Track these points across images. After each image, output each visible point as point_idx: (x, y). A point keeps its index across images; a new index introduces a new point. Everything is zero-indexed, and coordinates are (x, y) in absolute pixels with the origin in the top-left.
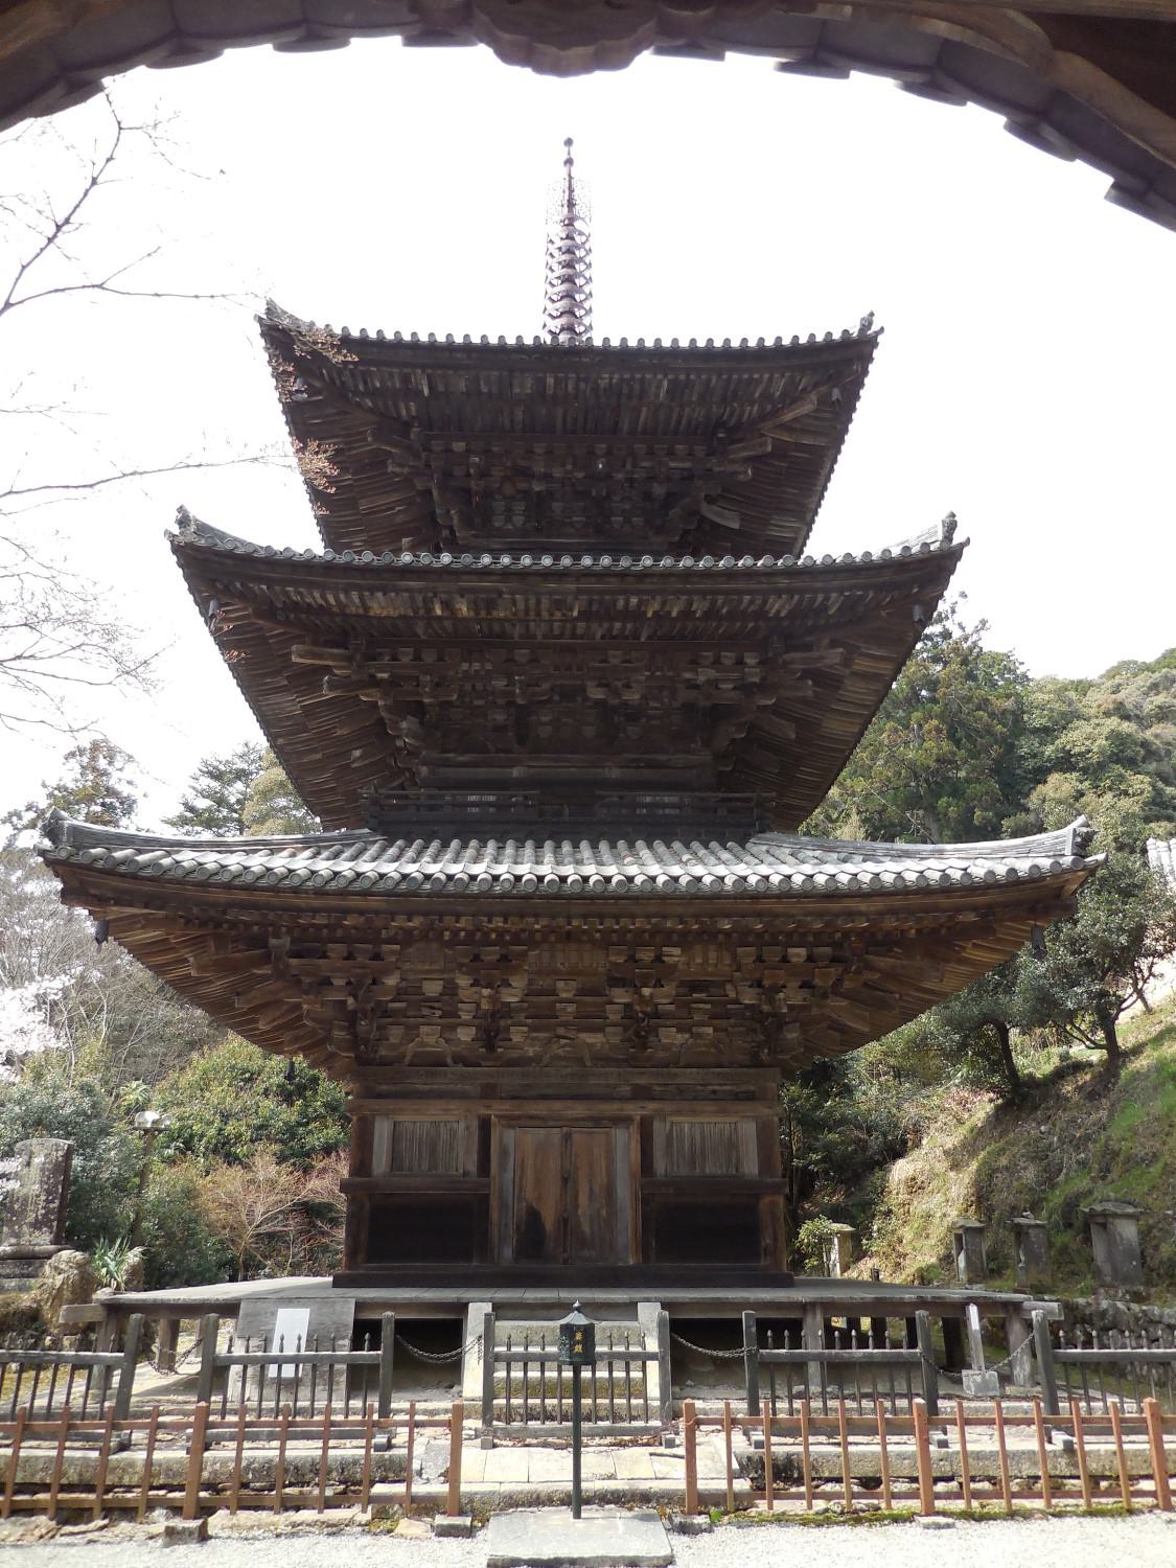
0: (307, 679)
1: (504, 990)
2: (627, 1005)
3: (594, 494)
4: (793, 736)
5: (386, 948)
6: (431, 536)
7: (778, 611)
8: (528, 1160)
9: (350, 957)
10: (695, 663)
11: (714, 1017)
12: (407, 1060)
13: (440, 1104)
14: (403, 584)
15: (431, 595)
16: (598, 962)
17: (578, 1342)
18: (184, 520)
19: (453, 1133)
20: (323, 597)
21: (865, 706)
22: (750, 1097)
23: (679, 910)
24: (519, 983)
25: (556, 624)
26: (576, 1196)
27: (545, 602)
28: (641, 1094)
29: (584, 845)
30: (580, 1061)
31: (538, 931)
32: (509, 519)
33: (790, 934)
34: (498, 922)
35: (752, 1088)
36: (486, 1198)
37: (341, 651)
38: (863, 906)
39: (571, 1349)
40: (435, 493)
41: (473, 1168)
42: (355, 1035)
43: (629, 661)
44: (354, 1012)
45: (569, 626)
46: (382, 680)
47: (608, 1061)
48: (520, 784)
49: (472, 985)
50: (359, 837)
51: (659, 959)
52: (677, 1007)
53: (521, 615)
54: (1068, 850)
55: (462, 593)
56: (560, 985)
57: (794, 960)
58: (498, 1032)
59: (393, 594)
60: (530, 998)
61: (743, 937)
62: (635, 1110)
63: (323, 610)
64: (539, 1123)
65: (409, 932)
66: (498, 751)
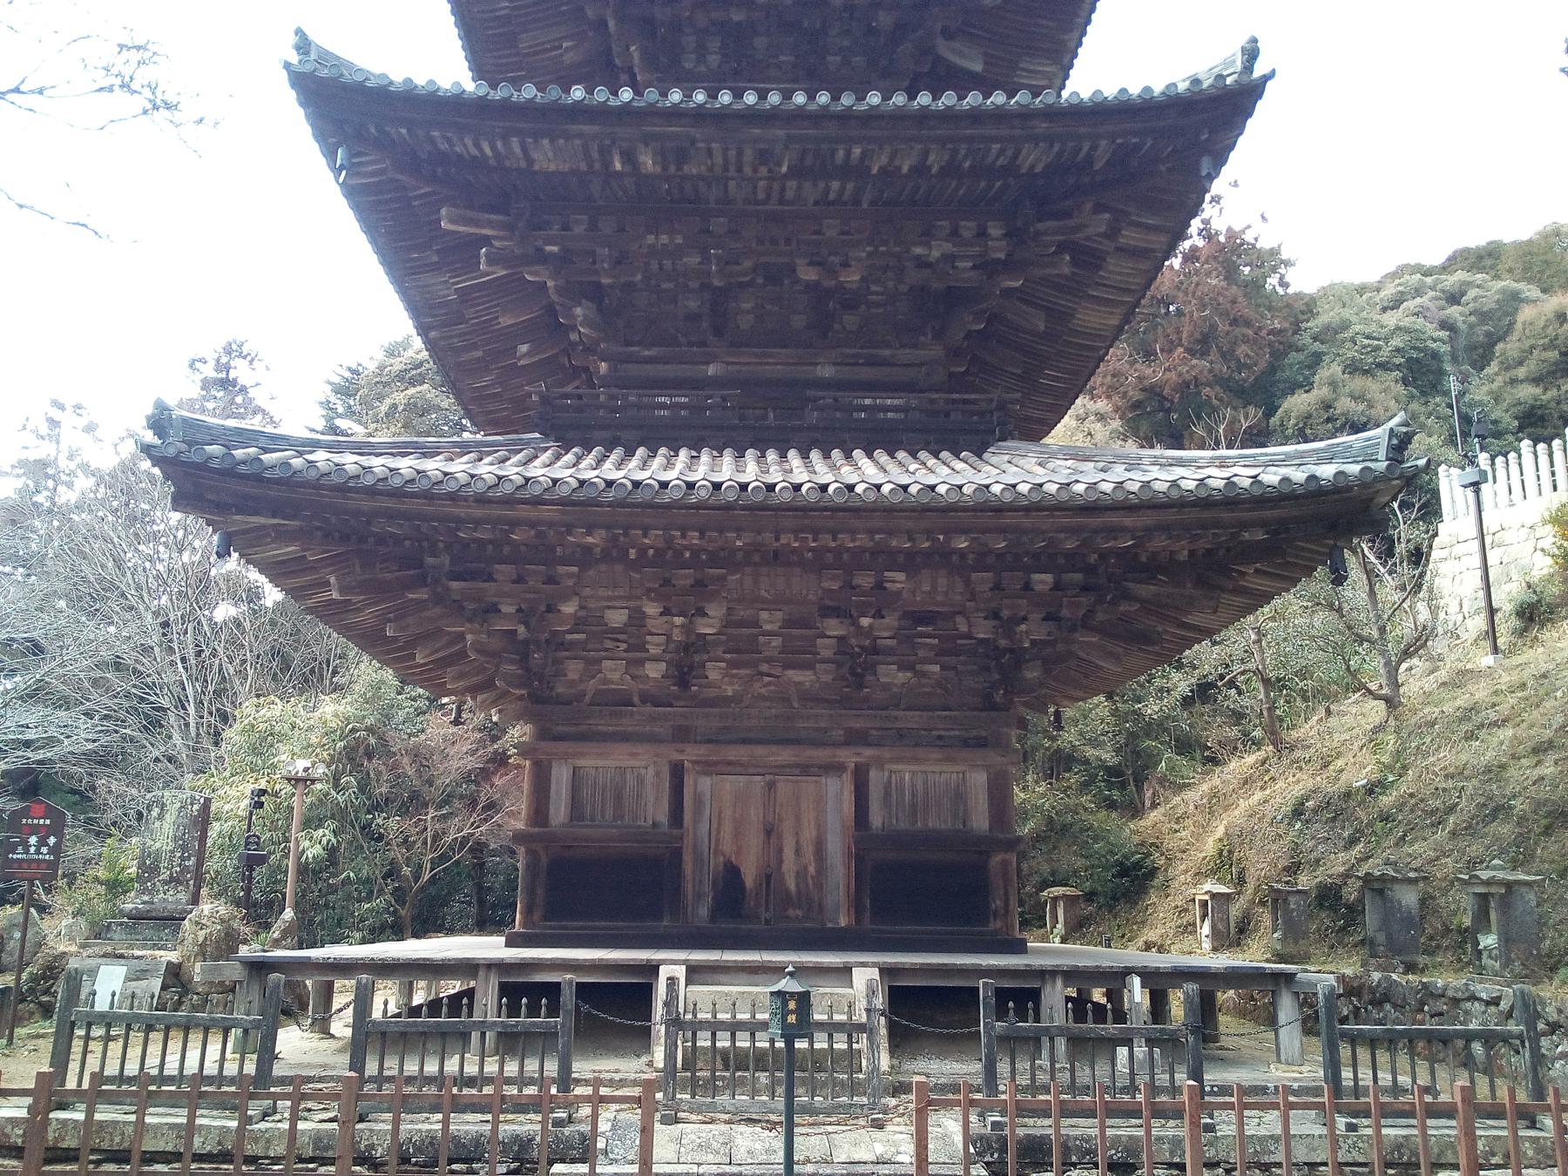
0: (461, 253)
1: (699, 620)
2: (841, 639)
3: (806, 25)
4: (1042, 327)
5: (562, 569)
6: (607, 71)
7: (1032, 167)
8: (729, 815)
9: (520, 580)
10: (927, 235)
11: (941, 652)
12: (587, 699)
13: (625, 748)
14: (575, 128)
15: (608, 142)
16: (806, 587)
17: (792, 1012)
18: (303, 44)
19: (641, 781)
20: (477, 146)
21: (1128, 291)
22: (982, 743)
23: (910, 524)
24: (716, 611)
25: (762, 183)
26: (780, 850)
27: (749, 155)
28: (856, 738)
29: (792, 453)
30: (786, 700)
31: (740, 549)
32: (701, 59)
33: (1036, 556)
34: (694, 538)
35: (984, 734)
36: (678, 853)
37: (500, 217)
38: (1128, 521)
39: (784, 1018)
40: (611, 24)
41: (663, 817)
42: (528, 670)
43: (847, 233)
44: (526, 643)
45: (776, 186)
46: (551, 254)
47: (818, 700)
48: (716, 383)
49: (662, 614)
50: (528, 442)
51: (879, 586)
52: (899, 643)
53: (718, 170)
54: (1382, 455)
55: (647, 139)
56: (764, 615)
57: (1038, 587)
58: (691, 668)
59: (562, 141)
60: (729, 631)
61: (983, 559)
62: (849, 757)
63: (478, 163)
64: (738, 769)
65: (588, 549)
66: (691, 344)
